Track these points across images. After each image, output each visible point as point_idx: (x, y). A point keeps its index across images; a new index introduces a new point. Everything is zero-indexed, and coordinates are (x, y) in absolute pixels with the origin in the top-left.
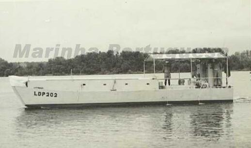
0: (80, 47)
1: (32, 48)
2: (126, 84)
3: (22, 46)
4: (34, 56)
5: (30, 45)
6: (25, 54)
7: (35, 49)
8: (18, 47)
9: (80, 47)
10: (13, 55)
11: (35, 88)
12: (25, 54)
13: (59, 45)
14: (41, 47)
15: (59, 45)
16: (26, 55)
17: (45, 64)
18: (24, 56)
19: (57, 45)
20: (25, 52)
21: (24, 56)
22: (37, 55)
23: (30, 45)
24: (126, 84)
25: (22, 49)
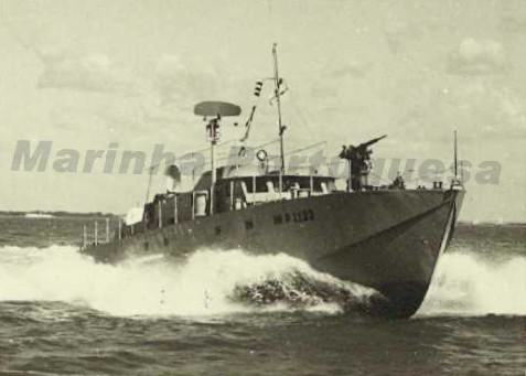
0: (165, 151)
1: (55, 149)
2: (236, 124)
3: (31, 143)
4: (290, 169)
5: (50, 143)
6: (38, 162)
7: (64, 152)
8: (23, 146)
9: (165, 151)
10: (10, 165)
11: (384, 137)
12: (38, 162)
13: (116, 145)
14: (75, 148)
15: (116, 145)
16: (86, 166)
17: (132, 256)
18: (36, 167)
19: (112, 145)
20: (40, 158)
21: (36, 167)
22: (65, 165)
23: (50, 143)
24: (236, 124)
25: (32, 151)
